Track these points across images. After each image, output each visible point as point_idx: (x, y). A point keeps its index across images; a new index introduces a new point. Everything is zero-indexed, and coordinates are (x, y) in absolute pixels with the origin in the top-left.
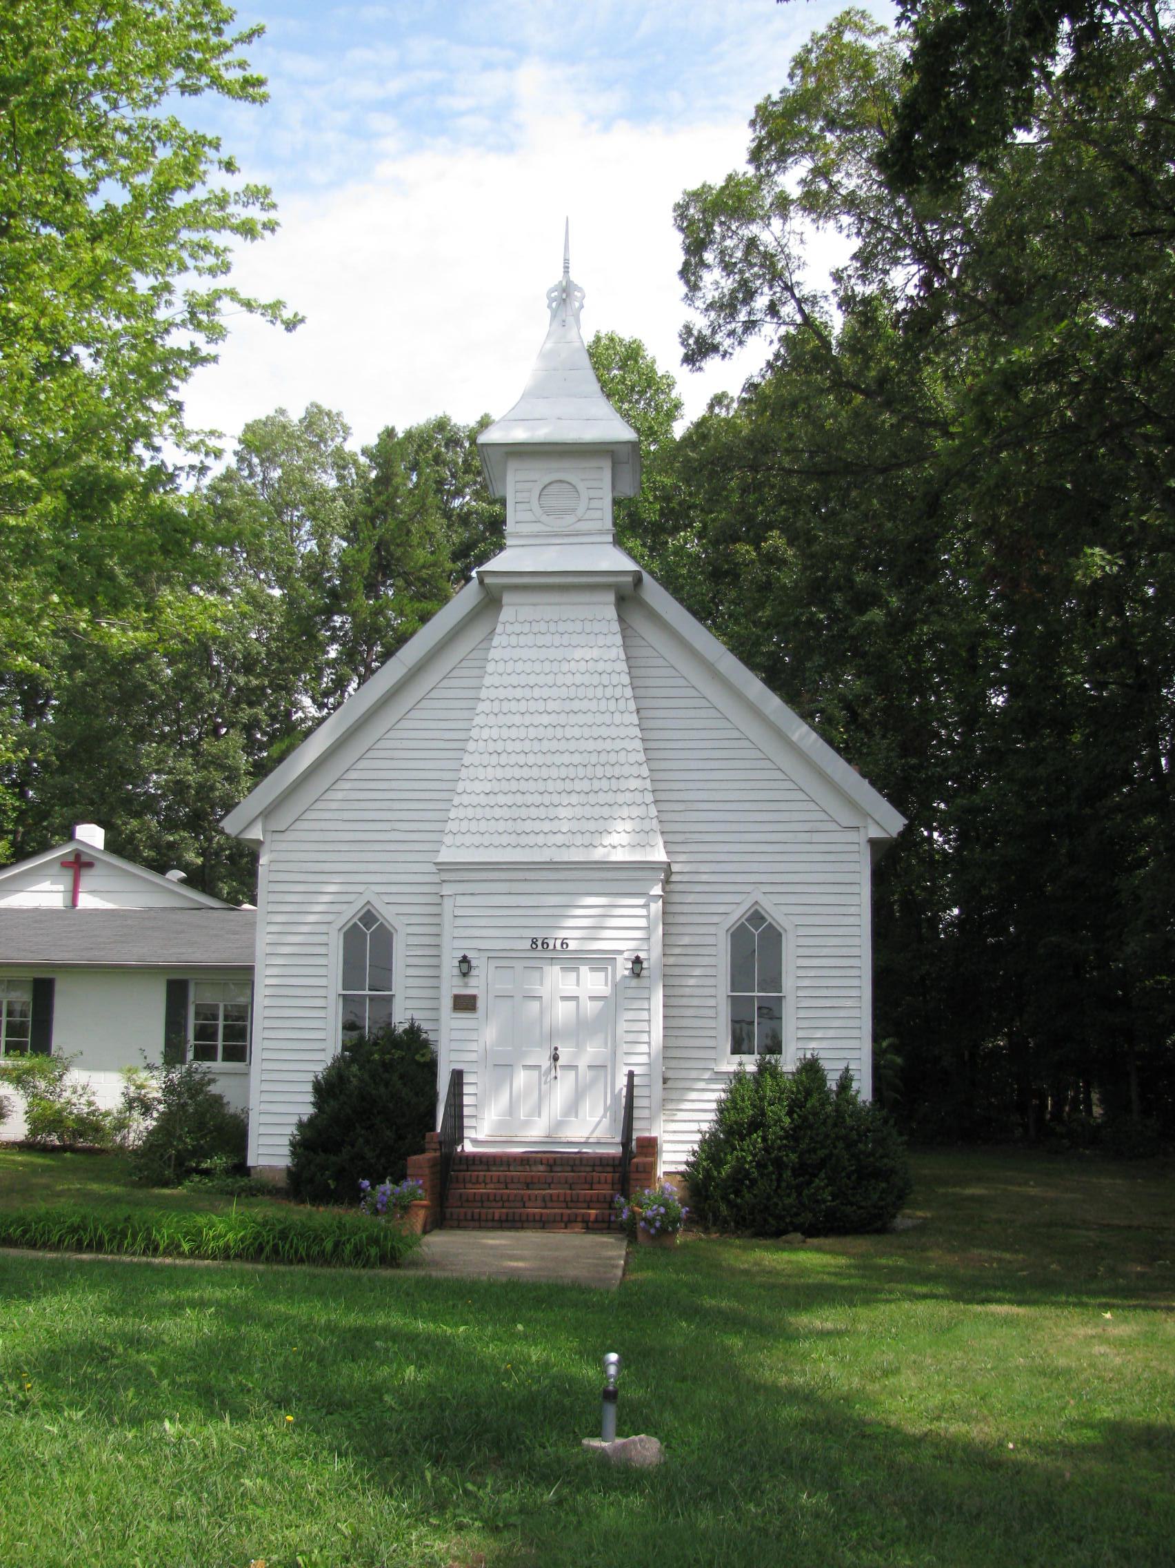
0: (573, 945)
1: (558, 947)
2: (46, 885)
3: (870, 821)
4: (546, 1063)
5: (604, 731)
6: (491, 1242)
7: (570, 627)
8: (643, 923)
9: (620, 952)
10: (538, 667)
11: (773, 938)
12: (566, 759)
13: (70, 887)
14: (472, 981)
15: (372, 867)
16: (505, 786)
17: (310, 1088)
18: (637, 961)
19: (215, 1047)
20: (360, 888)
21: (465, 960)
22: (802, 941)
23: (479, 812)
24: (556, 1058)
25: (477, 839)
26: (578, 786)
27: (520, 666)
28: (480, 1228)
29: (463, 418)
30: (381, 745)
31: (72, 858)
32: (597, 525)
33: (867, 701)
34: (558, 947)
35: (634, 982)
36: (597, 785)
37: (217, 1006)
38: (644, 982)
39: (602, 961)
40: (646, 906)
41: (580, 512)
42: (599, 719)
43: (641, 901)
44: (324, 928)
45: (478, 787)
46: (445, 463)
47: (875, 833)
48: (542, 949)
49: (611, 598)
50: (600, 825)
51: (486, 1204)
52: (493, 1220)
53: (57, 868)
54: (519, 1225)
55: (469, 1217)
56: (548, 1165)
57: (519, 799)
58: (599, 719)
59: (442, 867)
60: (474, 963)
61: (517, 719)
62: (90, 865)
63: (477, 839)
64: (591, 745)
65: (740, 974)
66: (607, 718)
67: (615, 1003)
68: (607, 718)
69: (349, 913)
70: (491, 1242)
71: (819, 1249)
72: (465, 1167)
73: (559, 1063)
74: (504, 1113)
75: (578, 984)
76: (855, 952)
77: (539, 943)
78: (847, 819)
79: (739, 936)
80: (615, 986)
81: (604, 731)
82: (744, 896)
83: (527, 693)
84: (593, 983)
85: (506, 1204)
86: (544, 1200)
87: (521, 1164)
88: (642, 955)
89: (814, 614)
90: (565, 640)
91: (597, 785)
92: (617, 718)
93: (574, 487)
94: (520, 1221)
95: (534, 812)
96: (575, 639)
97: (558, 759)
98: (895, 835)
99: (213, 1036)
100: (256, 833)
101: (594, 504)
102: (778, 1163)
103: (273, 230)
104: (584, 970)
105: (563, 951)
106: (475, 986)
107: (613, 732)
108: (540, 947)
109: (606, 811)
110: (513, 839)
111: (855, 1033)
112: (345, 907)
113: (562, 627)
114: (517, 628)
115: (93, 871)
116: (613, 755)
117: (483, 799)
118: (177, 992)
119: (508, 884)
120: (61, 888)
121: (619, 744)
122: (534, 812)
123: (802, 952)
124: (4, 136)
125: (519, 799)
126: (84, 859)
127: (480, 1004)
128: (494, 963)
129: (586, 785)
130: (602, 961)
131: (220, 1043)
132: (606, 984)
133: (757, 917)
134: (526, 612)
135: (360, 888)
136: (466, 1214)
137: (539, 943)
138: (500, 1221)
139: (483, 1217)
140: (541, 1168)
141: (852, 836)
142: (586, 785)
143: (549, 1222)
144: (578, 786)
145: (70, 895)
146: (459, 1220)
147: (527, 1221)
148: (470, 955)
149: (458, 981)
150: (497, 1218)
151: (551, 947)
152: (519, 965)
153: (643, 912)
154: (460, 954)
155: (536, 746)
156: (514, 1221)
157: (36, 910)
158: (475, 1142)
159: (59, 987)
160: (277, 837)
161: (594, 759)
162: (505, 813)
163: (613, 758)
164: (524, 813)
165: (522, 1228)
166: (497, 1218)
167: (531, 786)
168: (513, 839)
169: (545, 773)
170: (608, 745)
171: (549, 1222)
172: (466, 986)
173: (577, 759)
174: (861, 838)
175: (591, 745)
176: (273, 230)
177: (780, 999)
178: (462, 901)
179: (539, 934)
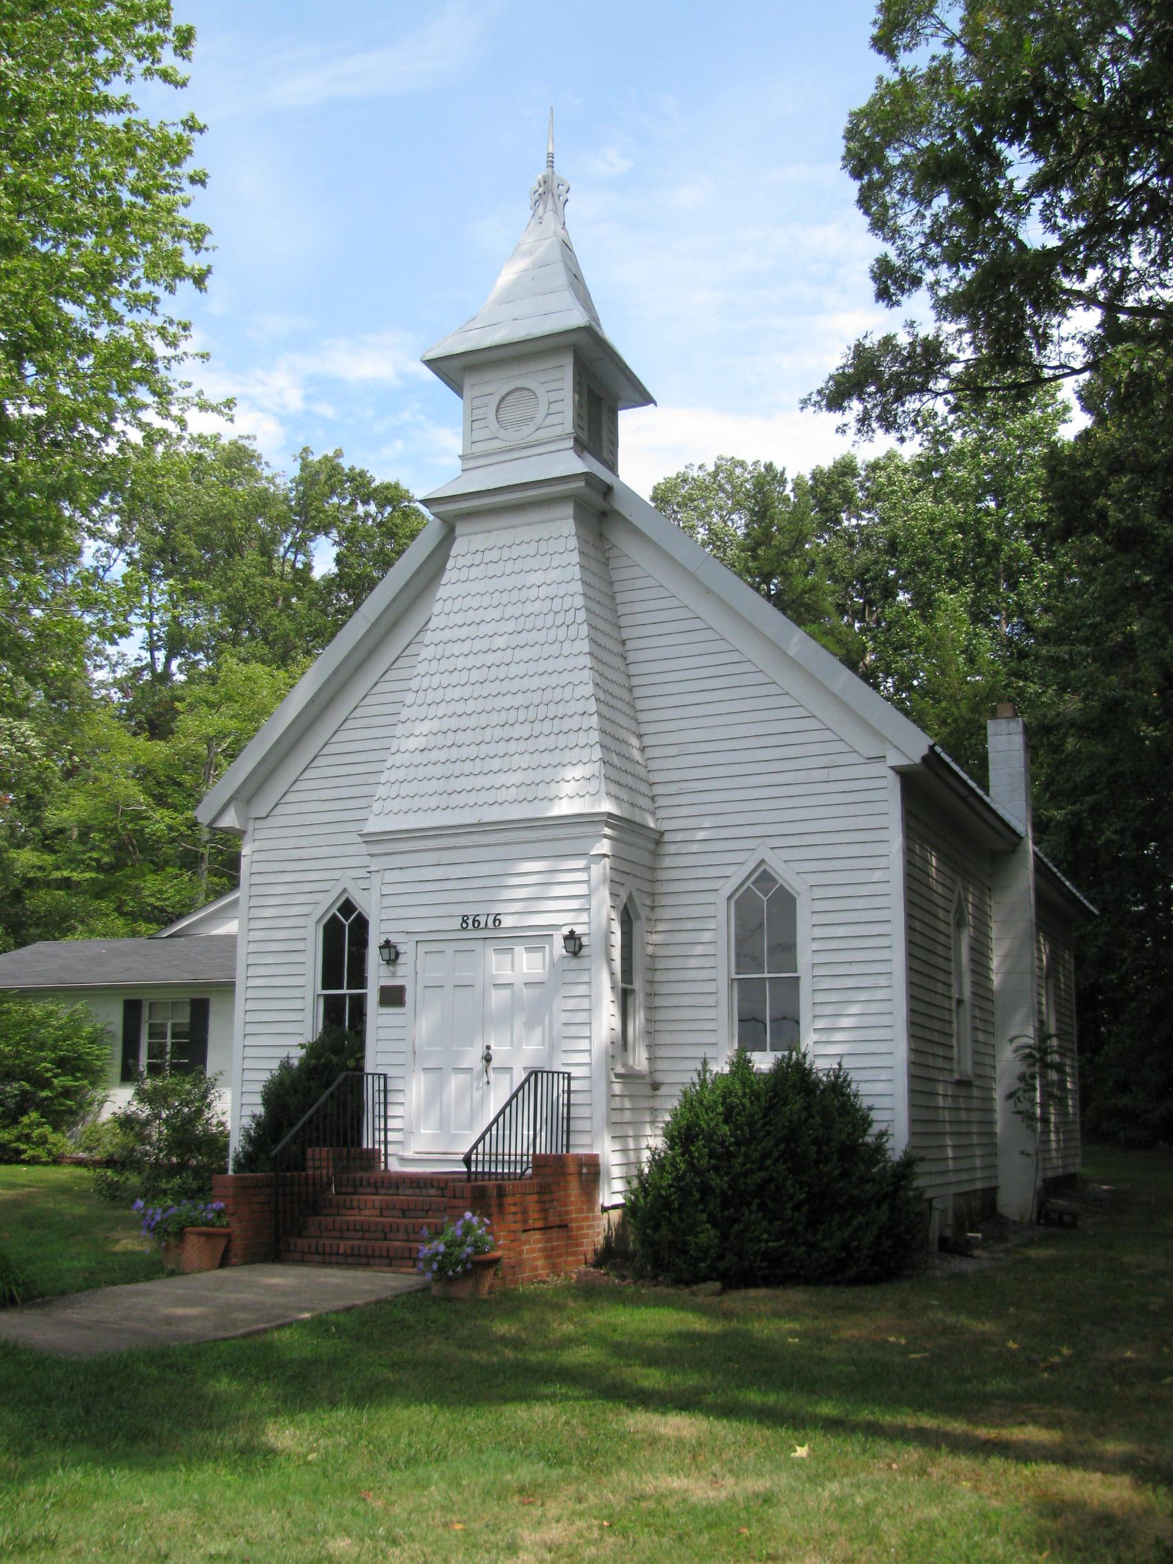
0: (507, 922)
1: (490, 923)
3: (888, 746)
4: (479, 1065)
5: (550, 665)
6: (275, 1281)
7: (524, 550)
8: (582, 890)
9: (558, 927)
10: (486, 601)
11: (785, 903)
12: (508, 701)
14: (400, 970)
16: (440, 740)
18: (571, 937)
20: (336, 874)
22: (819, 906)
23: (412, 772)
24: (488, 1059)
25: (405, 804)
26: (519, 731)
27: (468, 602)
28: (325, 1264)
29: (838, 457)
30: (358, 713)
32: (558, 431)
34: (490, 923)
35: (574, 963)
36: (537, 728)
38: (584, 963)
39: (536, 939)
40: (587, 869)
41: (538, 421)
42: (547, 651)
43: (581, 863)
44: (300, 922)
45: (413, 743)
46: (943, 533)
47: (901, 761)
48: (479, 928)
49: (569, 510)
50: (548, 774)
51: (346, 1234)
52: (338, 1254)
54: (364, 1260)
55: (313, 1250)
56: (439, 1188)
57: (454, 753)
58: (547, 651)
59: (371, 839)
60: (401, 948)
61: (461, 663)
63: (405, 804)
65: (745, 955)
66: (554, 649)
68: (554, 649)
69: (326, 904)
70: (275, 1281)
72: (350, 1190)
73: (494, 1064)
74: (425, 1122)
75: (513, 970)
76: (883, 915)
77: (470, 922)
79: (743, 904)
80: (553, 965)
81: (550, 665)
82: (747, 854)
83: (473, 631)
84: (527, 965)
85: (367, 1235)
86: (406, 1231)
87: (411, 1187)
88: (579, 930)
89: (1138, 577)
90: (518, 565)
91: (537, 728)
92: (567, 648)
93: (522, 389)
94: (366, 1256)
95: (468, 767)
96: (529, 564)
97: (499, 703)
98: (917, 759)
100: (230, 820)
101: (554, 408)
102: (705, 1189)
103: (203, 183)
104: (519, 950)
105: (496, 927)
106: (403, 976)
107: (560, 664)
108: (470, 926)
109: (546, 759)
110: (443, 801)
111: (885, 1020)
113: (516, 551)
114: (468, 560)
116: (559, 690)
117: (417, 758)
119: (437, 854)
121: (566, 677)
122: (468, 767)
123: (817, 919)
125: (454, 753)
127: (408, 997)
128: (422, 948)
129: (525, 730)
130: (536, 939)
132: (544, 968)
133: (764, 878)
134: (479, 542)
135: (336, 874)
136: (310, 1247)
137: (470, 922)
138: (345, 1255)
139: (328, 1250)
140: (433, 1192)
142: (525, 730)
143: (395, 1258)
144: (519, 731)
146: (303, 1253)
147: (374, 1256)
148: (394, 939)
149: (385, 970)
150: (341, 1251)
151: (483, 925)
152: (449, 948)
153: (582, 876)
155: (478, 690)
156: (359, 1255)
158: (403, 1160)
160: (259, 824)
161: (536, 697)
162: (439, 770)
163: (558, 694)
164: (458, 768)
165: (368, 1265)
166: (341, 1251)
167: (468, 737)
168: (443, 801)
169: (484, 720)
170: (554, 680)
171: (395, 1258)
172: (394, 975)
173: (519, 700)
174: (882, 769)
175: (535, 683)
176: (203, 183)
177: (798, 978)
178: (390, 876)
179: (470, 910)
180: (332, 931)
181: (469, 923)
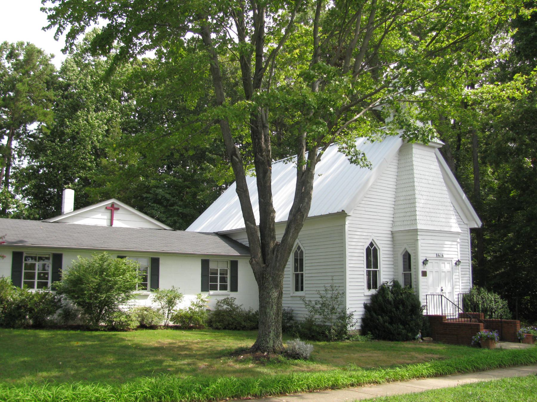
0: (445, 256)
2: (99, 216)
9: (453, 258)
13: (109, 217)
15: (373, 227)
17: (363, 306)
19: (217, 285)
20: (370, 234)
21: (426, 260)
24: (442, 290)
31: (110, 206)
33: (328, 140)
37: (217, 270)
43: (455, 243)
47: (476, 226)
53: (103, 210)
62: (118, 209)
64: (439, 195)
67: (452, 272)
71: (494, 376)
78: (466, 222)
97: (435, 199)
99: (33, 278)
112: (367, 240)
115: (119, 212)
118: (205, 263)
120: (106, 217)
124: (172, 1)
126: (115, 206)
130: (449, 261)
131: (36, 281)
135: (370, 234)
141: (466, 226)
145: (109, 221)
154: (424, 259)
157: (95, 227)
159: (161, 262)
179: (438, 252)
180: (368, 250)
181: (438, 255)
